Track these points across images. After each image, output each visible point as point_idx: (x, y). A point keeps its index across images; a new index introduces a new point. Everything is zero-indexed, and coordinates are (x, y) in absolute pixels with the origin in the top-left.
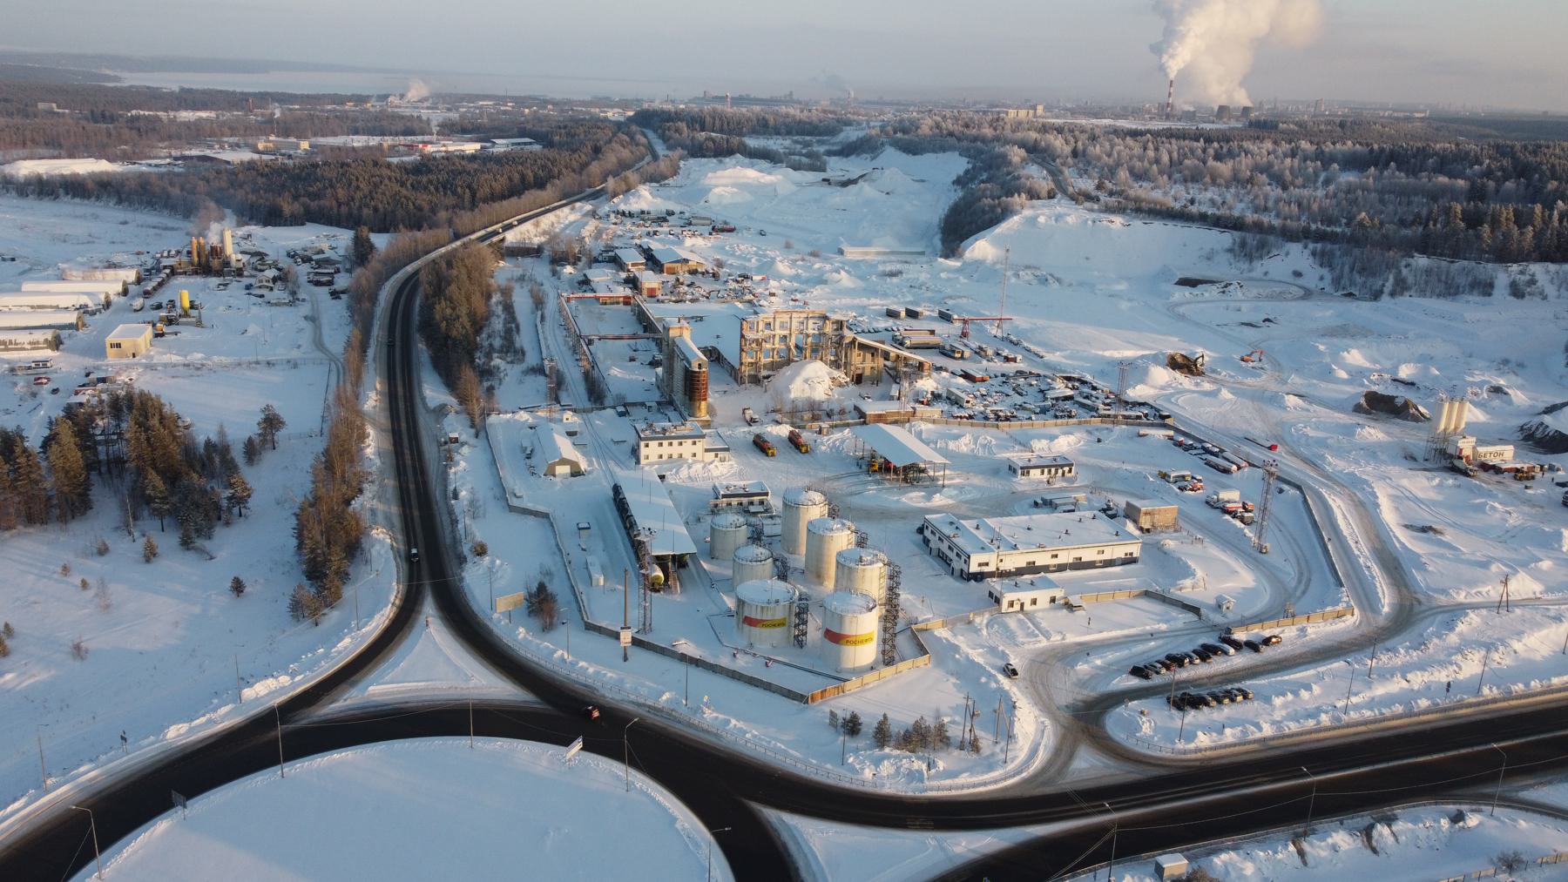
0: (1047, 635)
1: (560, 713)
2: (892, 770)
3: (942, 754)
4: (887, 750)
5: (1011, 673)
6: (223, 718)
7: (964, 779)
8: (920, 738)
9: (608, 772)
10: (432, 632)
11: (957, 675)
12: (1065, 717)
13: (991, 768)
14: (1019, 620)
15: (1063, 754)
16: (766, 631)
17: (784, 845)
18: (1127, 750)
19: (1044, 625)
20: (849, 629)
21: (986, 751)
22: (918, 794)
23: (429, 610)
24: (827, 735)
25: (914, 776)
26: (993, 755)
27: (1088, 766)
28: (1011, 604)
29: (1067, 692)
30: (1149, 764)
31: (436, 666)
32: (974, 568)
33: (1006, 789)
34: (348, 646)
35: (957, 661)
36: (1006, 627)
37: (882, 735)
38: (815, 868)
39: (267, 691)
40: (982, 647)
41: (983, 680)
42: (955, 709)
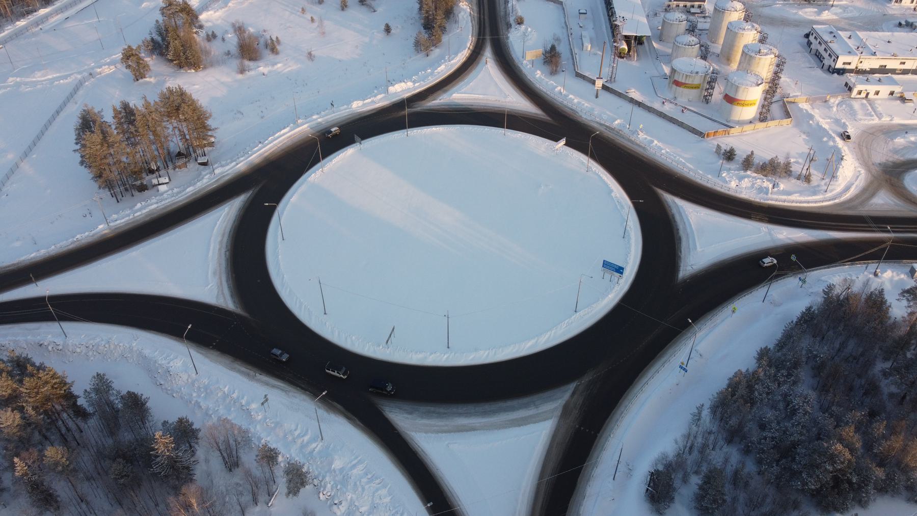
0: (880, 116)
1: (556, 123)
2: (749, 185)
3: (785, 181)
4: (749, 173)
6: (379, 101)
8: (771, 169)
9: (578, 160)
10: (488, 67)
15: (868, 191)
19: (880, 109)
20: (741, 96)
23: (488, 54)
25: (761, 190)
27: (883, 202)
28: (860, 93)
29: (883, 154)
31: (488, 87)
32: (839, 65)
33: (822, 207)
34: (444, 70)
35: (811, 125)
36: (851, 107)
39: (402, 89)
40: (830, 118)
41: (825, 139)
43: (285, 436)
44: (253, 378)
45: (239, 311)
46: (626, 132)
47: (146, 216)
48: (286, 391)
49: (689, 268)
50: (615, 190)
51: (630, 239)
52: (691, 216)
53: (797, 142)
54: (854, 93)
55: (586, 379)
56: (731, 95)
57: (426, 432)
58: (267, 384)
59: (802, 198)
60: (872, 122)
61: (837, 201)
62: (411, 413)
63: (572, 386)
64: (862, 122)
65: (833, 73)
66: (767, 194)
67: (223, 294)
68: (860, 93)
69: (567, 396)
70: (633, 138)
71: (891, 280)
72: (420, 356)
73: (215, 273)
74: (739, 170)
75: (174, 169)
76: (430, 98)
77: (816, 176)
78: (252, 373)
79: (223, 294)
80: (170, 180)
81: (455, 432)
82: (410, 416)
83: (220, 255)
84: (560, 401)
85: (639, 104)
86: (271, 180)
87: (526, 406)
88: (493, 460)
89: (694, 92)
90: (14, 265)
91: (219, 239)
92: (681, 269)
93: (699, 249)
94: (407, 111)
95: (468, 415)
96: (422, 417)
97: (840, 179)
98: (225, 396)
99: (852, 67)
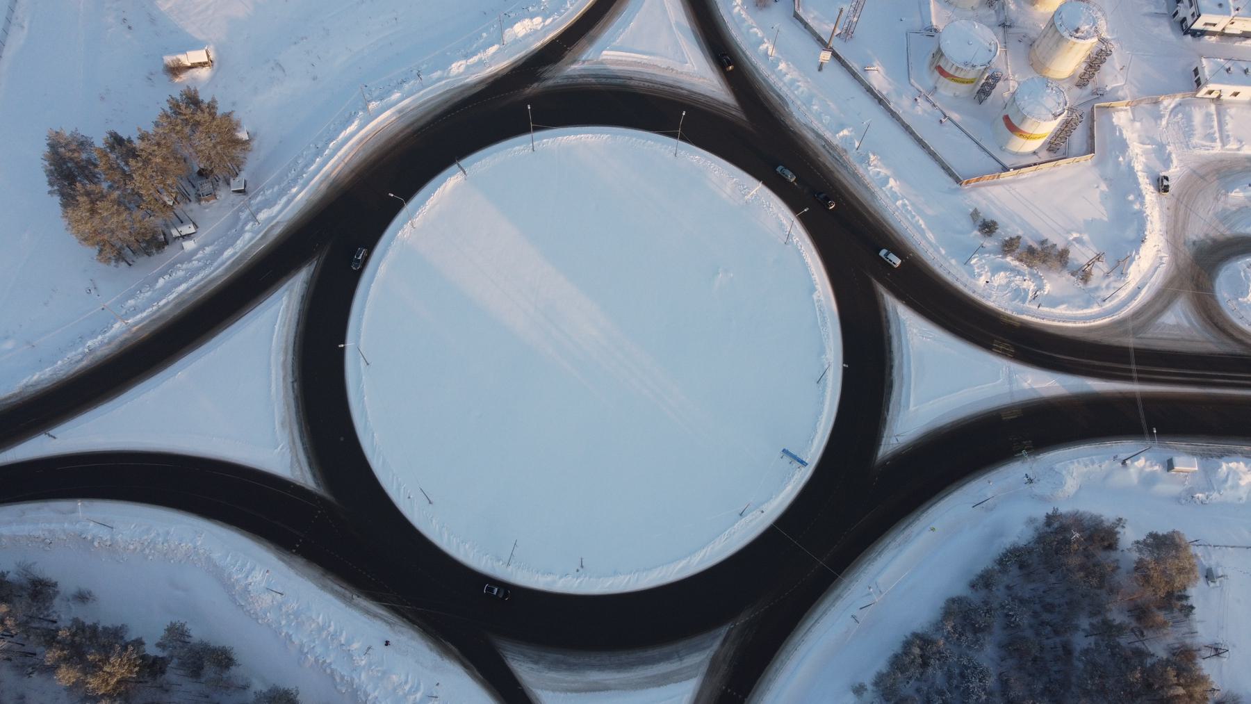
0: (1224, 140)
2: (1004, 282)
3: (1055, 276)
4: (1009, 259)
5: (1162, 185)
7: (1061, 310)
8: (1042, 255)
9: (777, 217)
11: (1110, 181)
12: (1187, 252)
13: (1088, 304)
14: (1208, 115)
15: (1163, 299)
16: (952, 84)
17: (890, 338)
18: (1220, 313)
19: (1229, 127)
20: (1027, 127)
21: (1092, 283)
22: (1015, 314)
24: (966, 223)
25: (1019, 294)
26: (1097, 289)
27: (1178, 325)
28: (1210, 92)
29: (1201, 227)
30: (1231, 336)
32: (1198, 25)
33: (1090, 330)
35: (1119, 164)
36: (1189, 118)
37: (1009, 246)
38: (905, 351)
40: (1152, 141)
41: (1131, 198)
42: (1089, 225)
43: (395, 689)
44: (349, 602)
45: (321, 491)
46: (851, 157)
47: (177, 305)
48: (389, 624)
49: (893, 441)
50: (819, 287)
51: (825, 385)
52: (915, 335)
53: (1081, 227)
54: (1202, 92)
55: (742, 620)
56: (1015, 121)
57: (553, 690)
58: (367, 612)
59: (1069, 313)
60: (1212, 152)
61: (1116, 317)
62: (536, 663)
63: (724, 630)
64: (1197, 152)
65: (1185, 33)
66: (1024, 300)
67: (298, 461)
68: (1210, 92)
69: (716, 645)
70: (861, 170)
71: (1141, 470)
72: (549, 579)
73: (283, 424)
74: (996, 253)
75: (199, 200)
76: (568, 56)
77: (1098, 271)
78: (348, 594)
79: (298, 461)
80: (196, 227)
81: (586, 691)
82: (535, 667)
83: (285, 387)
84: (708, 652)
85: (881, 101)
86: (337, 237)
87: (667, 658)
88: (652, 43)
89: (963, 88)
90: (15, 395)
91: (281, 359)
92: (884, 441)
93: (912, 408)
94: (535, 88)
95: (602, 667)
96: (550, 669)
97: (1130, 277)
98: (321, 629)
99: (1218, 29)
